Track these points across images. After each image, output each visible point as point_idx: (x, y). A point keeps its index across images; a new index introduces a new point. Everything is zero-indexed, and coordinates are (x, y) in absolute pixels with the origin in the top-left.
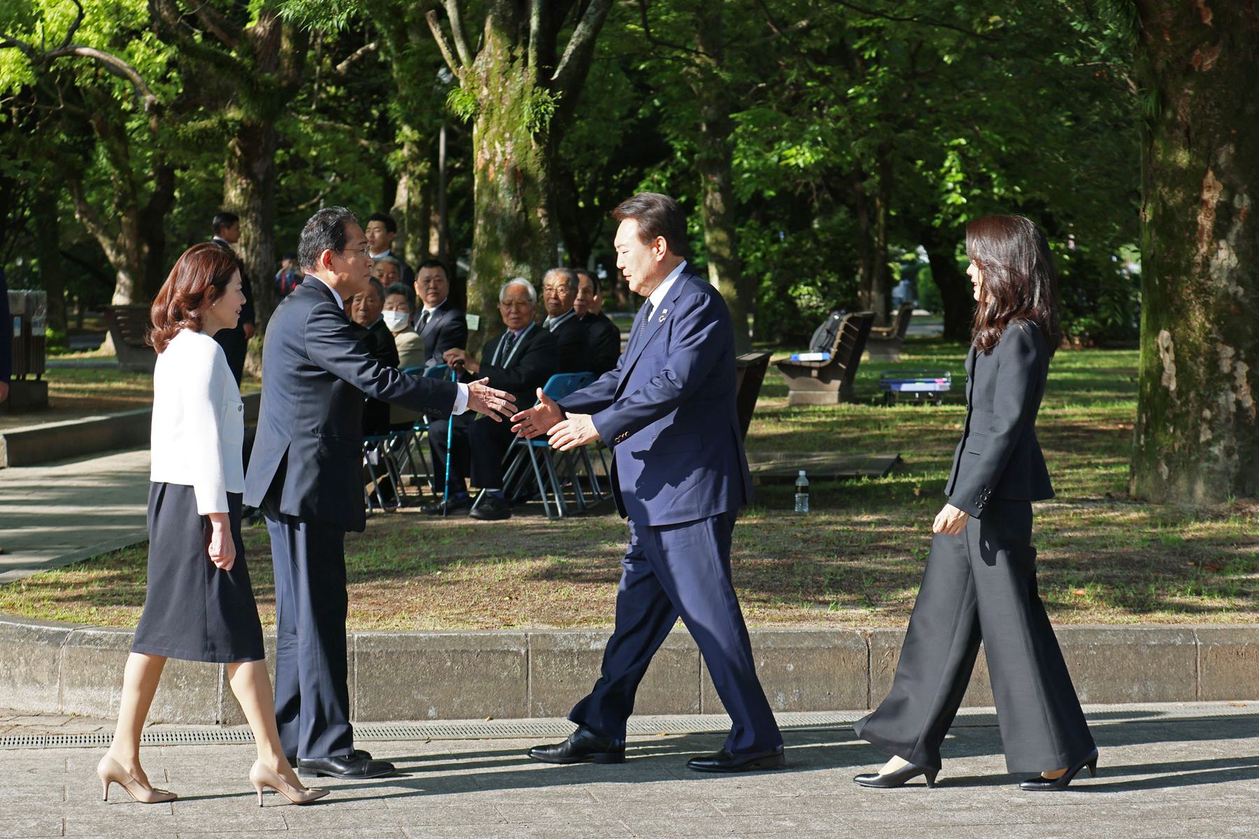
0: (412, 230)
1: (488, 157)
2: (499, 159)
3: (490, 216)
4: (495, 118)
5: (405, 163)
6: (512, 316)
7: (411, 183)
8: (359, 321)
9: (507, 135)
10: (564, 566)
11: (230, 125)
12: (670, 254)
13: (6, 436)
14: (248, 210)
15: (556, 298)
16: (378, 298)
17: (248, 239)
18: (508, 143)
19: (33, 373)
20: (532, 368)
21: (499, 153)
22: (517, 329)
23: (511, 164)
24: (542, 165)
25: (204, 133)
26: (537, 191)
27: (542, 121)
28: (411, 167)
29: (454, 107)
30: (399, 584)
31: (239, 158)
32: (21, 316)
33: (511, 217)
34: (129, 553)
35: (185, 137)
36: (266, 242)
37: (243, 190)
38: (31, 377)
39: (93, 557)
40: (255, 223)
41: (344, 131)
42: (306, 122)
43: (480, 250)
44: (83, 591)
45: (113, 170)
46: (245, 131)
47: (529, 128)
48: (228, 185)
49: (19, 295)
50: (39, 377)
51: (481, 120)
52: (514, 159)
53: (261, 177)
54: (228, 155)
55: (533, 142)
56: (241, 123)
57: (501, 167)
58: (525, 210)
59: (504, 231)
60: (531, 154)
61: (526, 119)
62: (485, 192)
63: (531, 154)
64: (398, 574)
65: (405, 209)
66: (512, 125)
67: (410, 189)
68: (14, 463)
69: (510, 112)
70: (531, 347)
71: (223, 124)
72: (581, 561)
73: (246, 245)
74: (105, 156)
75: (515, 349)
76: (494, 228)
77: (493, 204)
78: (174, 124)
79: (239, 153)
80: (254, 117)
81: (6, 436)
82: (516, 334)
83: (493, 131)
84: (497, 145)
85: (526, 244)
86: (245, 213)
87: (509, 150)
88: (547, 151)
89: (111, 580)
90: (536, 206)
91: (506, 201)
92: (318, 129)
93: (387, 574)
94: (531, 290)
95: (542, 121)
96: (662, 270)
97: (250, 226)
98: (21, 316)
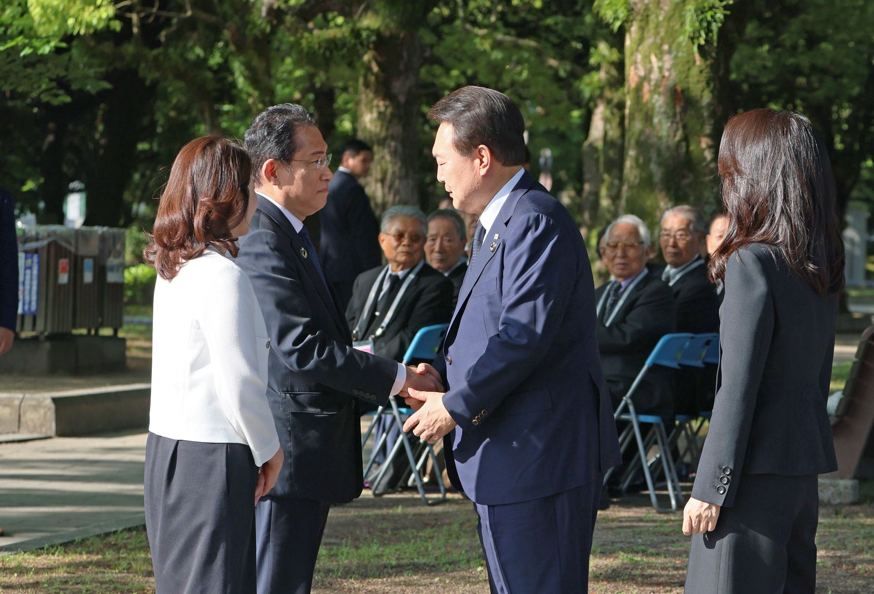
0: (608, 170)
1: (642, 73)
2: (655, 76)
3: (643, 145)
4: (652, 26)
5: (602, 88)
6: (618, 261)
7: (608, 113)
8: (435, 265)
9: (666, 47)
10: (636, 565)
11: (364, 34)
12: (498, 165)
13: (55, 400)
14: (385, 139)
15: (675, 245)
16: (457, 237)
17: (384, 173)
18: (666, 57)
19: (108, 326)
20: (639, 326)
21: (656, 69)
22: (625, 277)
23: (670, 83)
24: (708, 84)
25: (333, 45)
26: (701, 117)
27: (709, 30)
28: (608, 94)
29: (602, 12)
30: (427, 581)
31: (376, 76)
32: (94, 258)
33: (668, 148)
34: (126, 535)
35: (310, 48)
36: (406, 176)
37: (380, 113)
38: (106, 332)
39: (78, 539)
40: (394, 153)
41: (529, 49)
42: (484, 37)
43: (631, 187)
44: (44, 577)
45: (251, 90)
46: (382, 43)
47: (692, 39)
48: (363, 108)
49: (91, 233)
50: (116, 331)
51: (634, 28)
52: (672, 76)
53: (402, 99)
54: (363, 72)
55: (697, 57)
56: (377, 33)
57: (657, 86)
58: (686, 139)
59: (660, 164)
60: (694, 71)
61: (688, 28)
62: (639, 117)
63: (694, 71)
64: (432, 569)
65: (600, 145)
66: (672, 35)
67: (606, 120)
68: (62, 433)
69: (669, 19)
70: (640, 302)
71: (356, 33)
72: (661, 560)
73: (383, 181)
74: (242, 74)
75: (621, 303)
76: (648, 161)
77: (648, 131)
78: (296, 31)
79: (375, 68)
80: (392, 25)
81: (55, 400)
82: (624, 284)
83: (649, 41)
84: (654, 59)
85: (686, 181)
86: (382, 142)
87: (667, 65)
88: (714, 68)
89: (85, 565)
90: (699, 134)
91: (664, 129)
92: (497, 45)
93: (416, 568)
94: (643, 231)
95: (709, 30)
96: (488, 186)
97: (388, 158)
98: (94, 258)
